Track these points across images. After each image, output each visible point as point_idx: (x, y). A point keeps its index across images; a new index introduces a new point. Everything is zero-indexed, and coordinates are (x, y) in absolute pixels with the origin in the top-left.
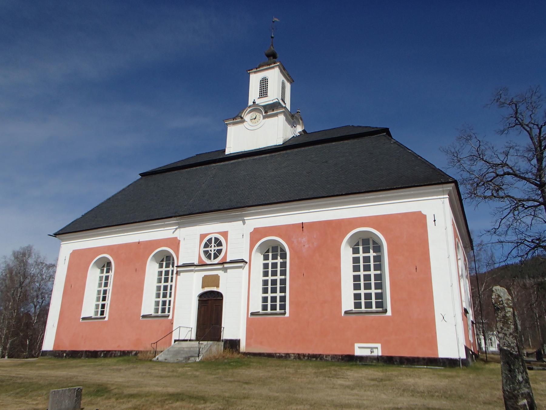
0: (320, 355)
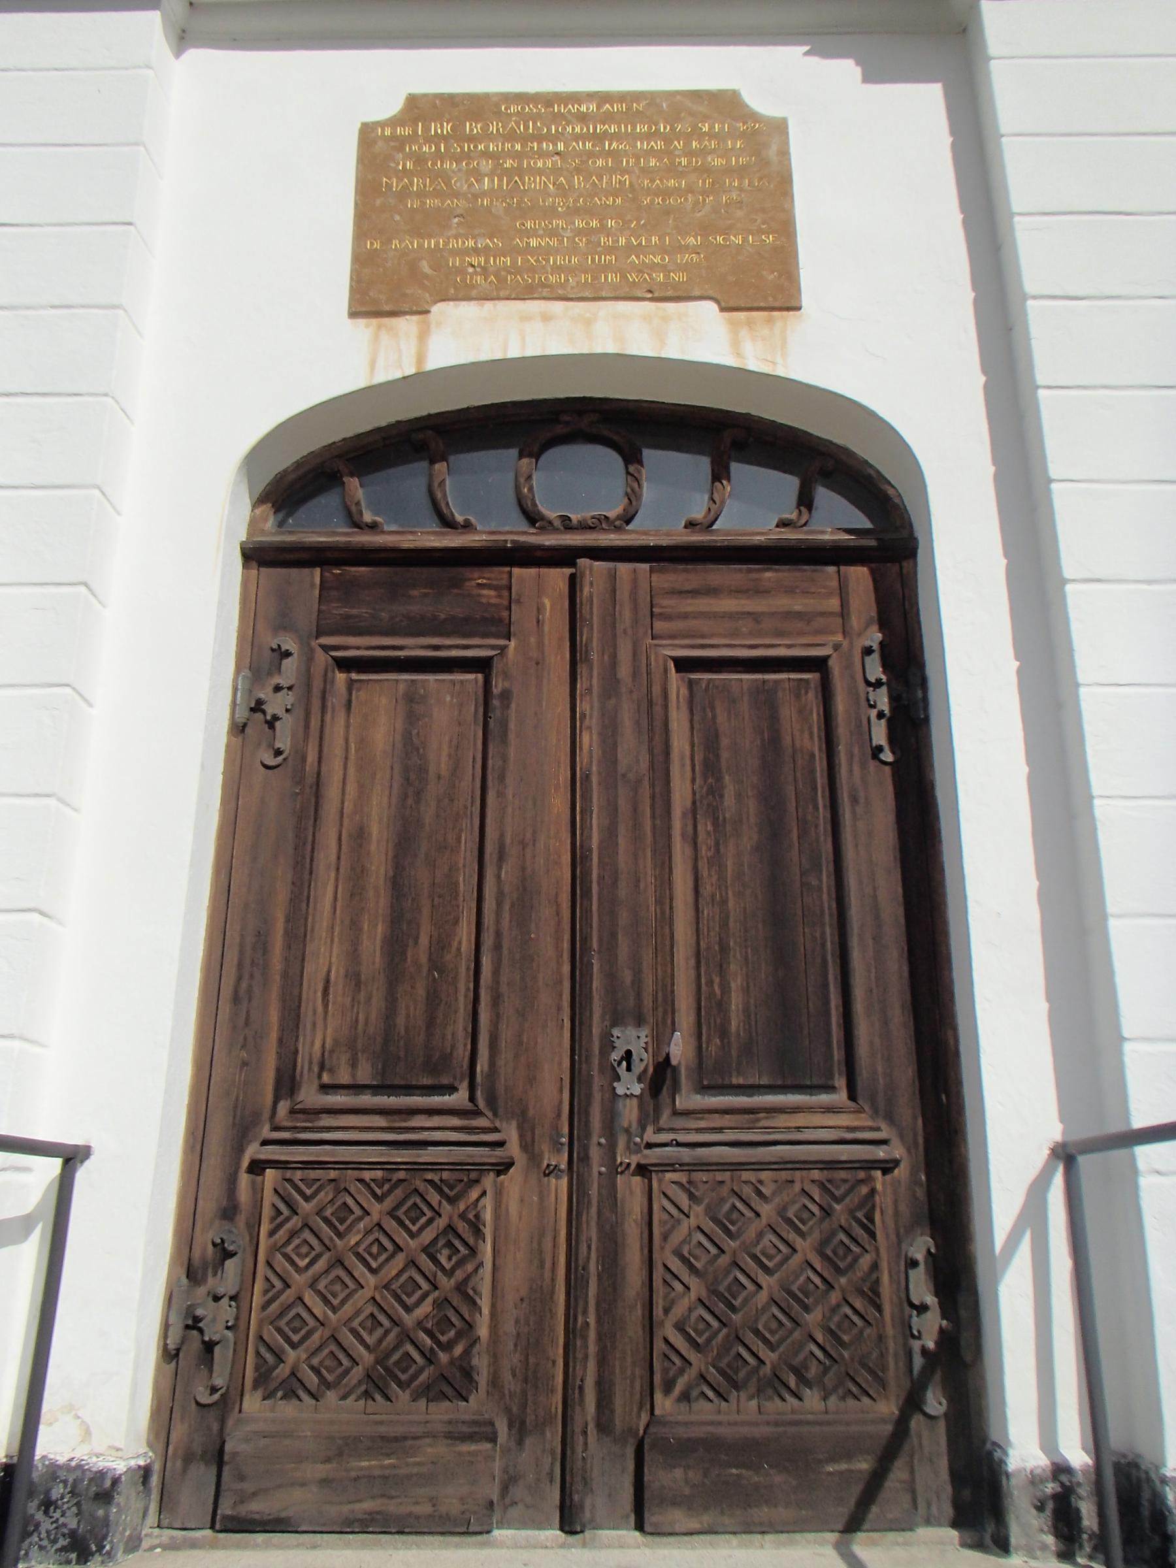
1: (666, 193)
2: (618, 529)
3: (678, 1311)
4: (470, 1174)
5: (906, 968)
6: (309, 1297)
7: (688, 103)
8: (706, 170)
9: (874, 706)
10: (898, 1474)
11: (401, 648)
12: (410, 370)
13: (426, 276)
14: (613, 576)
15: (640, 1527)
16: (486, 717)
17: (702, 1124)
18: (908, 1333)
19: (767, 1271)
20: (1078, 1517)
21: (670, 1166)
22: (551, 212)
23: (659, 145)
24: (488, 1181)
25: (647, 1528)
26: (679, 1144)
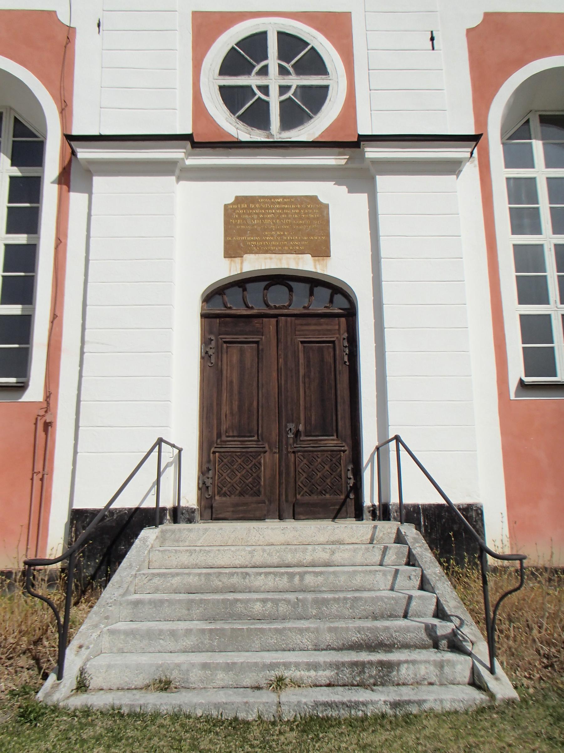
0: (106, 586)
1: (299, 225)
2: (288, 309)
3: (302, 479)
4: (258, 454)
5: (349, 410)
6: (227, 478)
7: (305, 199)
8: (308, 218)
9: (345, 352)
10: (344, 509)
11: (238, 338)
12: (239, 272)
13: (242, 247)
14: (286, 322)
15: (294, 519)
16: (258, 355)
17: (306, 443)
18: (347, 483)
19: (319, 472)
20: (376, 514)
21: (299, 451)
22: (271, 230)
23: (297, 211)
24: (262, 455)
25: (295, 518)
26: (301, 447)
